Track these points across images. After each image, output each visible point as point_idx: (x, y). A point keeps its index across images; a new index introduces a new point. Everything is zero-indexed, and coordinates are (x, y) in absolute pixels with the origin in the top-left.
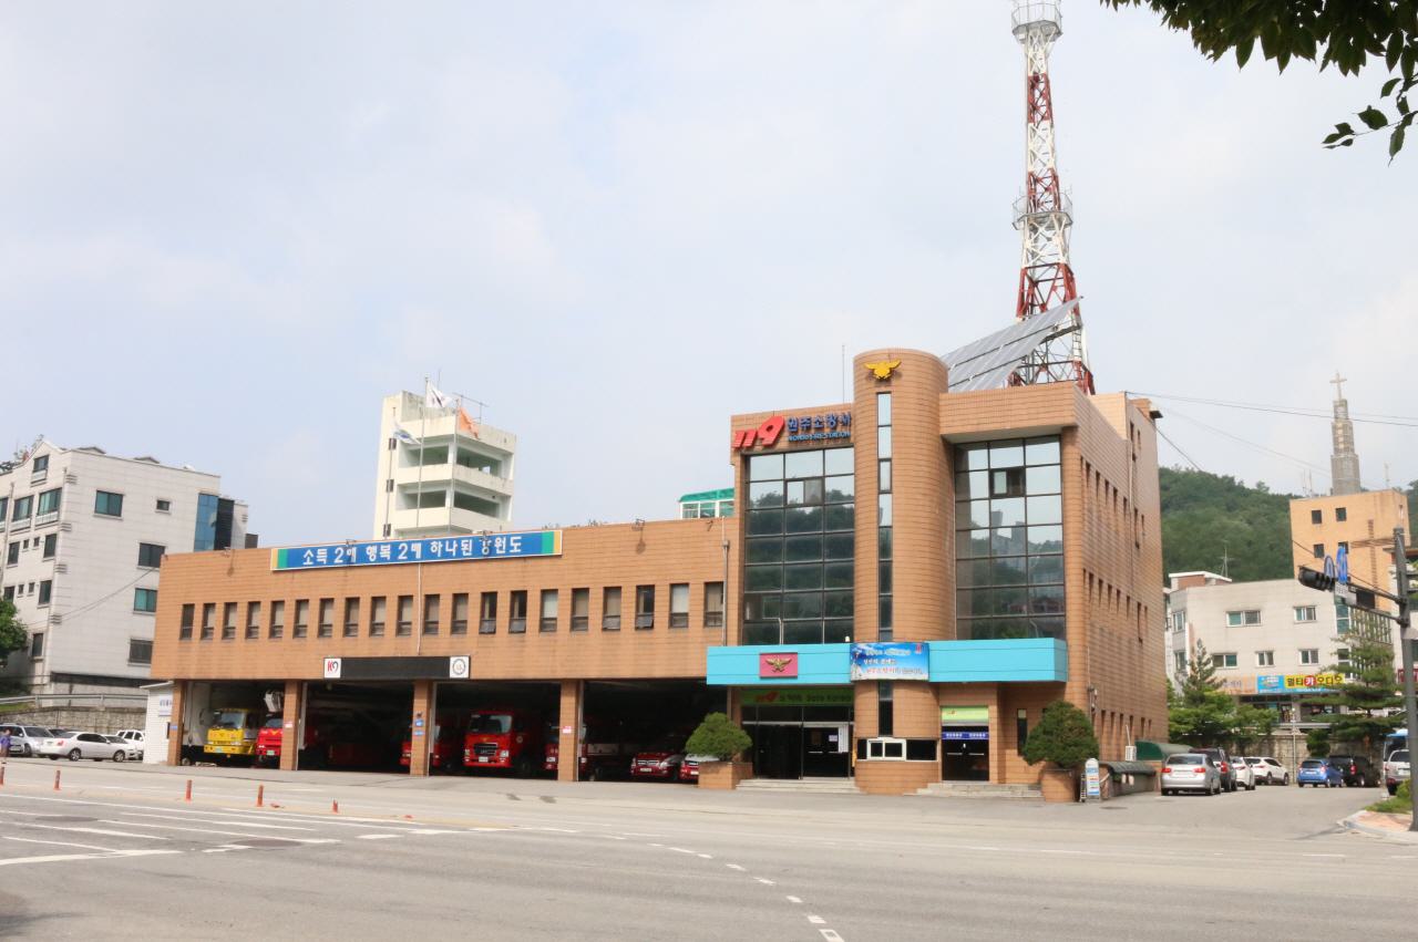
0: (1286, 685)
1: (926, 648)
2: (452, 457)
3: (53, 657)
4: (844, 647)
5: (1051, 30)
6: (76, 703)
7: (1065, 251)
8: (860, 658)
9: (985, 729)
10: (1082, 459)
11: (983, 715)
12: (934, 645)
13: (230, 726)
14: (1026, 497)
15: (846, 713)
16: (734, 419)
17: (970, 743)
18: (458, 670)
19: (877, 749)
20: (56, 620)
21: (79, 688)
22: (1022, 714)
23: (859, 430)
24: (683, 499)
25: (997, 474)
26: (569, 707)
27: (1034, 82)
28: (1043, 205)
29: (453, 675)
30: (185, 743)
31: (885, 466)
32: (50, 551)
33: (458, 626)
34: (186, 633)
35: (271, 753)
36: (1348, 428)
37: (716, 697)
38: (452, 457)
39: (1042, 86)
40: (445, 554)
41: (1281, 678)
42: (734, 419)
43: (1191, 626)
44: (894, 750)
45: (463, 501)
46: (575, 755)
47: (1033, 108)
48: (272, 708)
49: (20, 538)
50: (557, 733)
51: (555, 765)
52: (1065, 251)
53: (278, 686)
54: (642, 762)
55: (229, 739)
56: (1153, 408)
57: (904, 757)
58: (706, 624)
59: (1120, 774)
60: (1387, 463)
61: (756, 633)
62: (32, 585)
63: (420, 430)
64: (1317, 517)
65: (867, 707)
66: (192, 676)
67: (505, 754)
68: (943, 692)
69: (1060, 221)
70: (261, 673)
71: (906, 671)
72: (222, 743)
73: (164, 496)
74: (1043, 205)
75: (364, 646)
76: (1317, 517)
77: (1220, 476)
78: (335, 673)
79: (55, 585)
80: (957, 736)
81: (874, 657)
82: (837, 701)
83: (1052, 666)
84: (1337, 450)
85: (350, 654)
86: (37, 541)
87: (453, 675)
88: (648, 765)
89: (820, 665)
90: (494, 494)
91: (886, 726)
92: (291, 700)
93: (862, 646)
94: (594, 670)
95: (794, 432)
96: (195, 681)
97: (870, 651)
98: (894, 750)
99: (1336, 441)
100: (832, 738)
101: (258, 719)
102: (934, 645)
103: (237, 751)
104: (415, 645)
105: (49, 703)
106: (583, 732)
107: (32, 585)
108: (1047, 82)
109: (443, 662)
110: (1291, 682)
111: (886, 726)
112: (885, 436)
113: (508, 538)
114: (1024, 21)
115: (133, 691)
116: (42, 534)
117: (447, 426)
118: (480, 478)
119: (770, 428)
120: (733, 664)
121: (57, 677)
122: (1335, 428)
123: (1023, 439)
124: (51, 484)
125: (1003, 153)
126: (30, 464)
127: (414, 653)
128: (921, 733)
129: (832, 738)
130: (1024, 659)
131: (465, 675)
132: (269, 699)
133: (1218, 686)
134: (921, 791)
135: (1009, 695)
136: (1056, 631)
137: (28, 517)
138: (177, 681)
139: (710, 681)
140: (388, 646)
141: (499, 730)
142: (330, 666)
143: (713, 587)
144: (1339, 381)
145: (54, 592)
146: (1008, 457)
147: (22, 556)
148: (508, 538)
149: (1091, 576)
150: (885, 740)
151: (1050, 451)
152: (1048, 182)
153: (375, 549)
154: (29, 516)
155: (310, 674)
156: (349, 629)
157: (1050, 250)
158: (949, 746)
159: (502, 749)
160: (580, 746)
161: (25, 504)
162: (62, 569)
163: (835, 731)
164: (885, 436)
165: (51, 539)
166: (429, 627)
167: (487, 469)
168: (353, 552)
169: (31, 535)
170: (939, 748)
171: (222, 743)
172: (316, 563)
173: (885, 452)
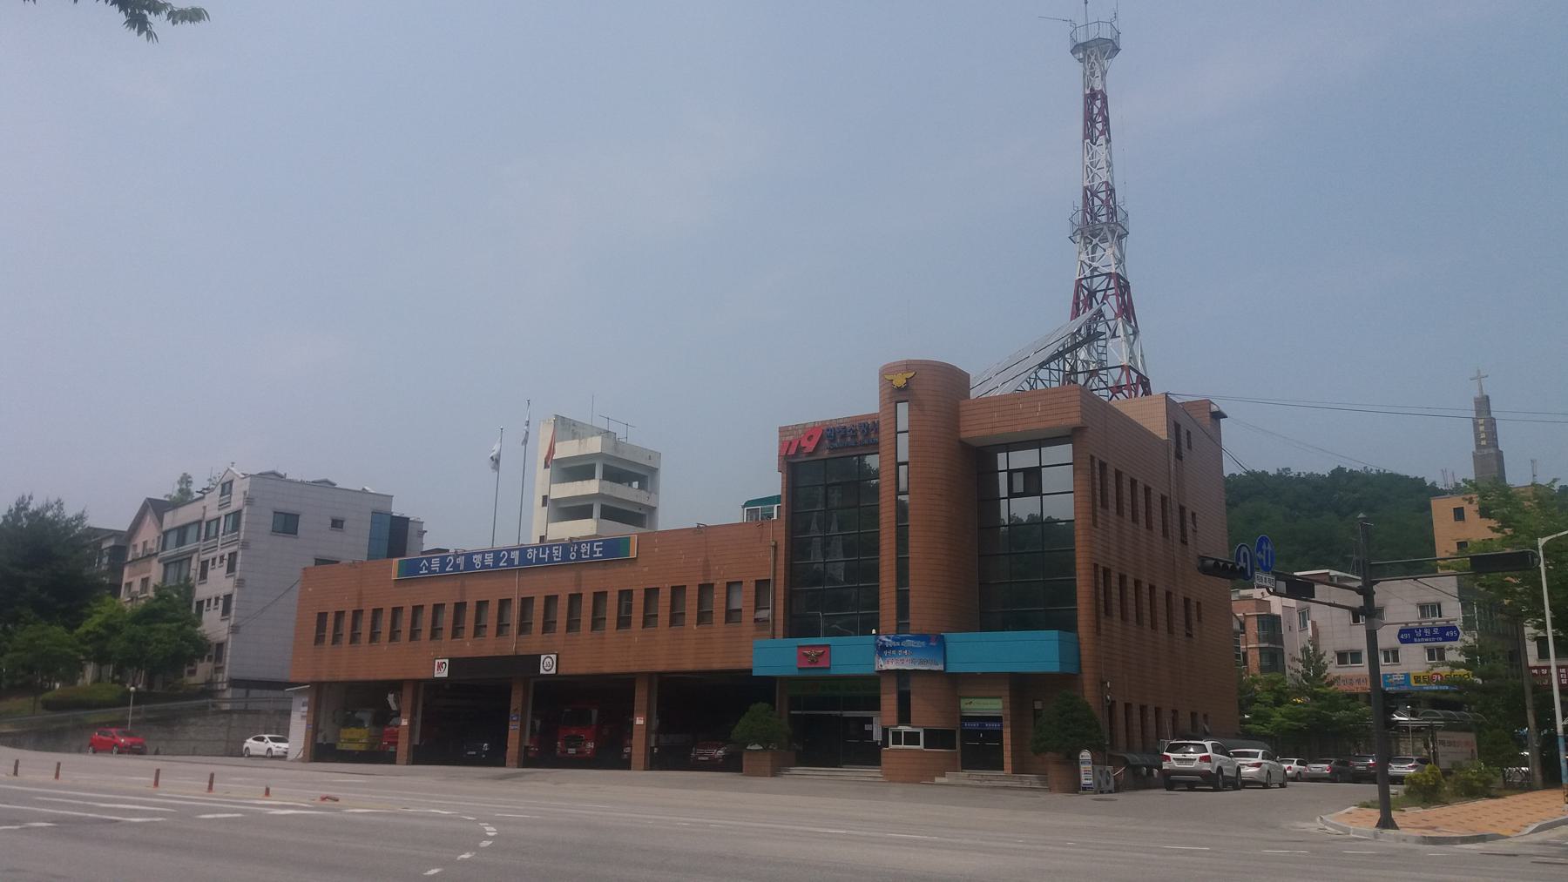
0: (1413, 682)
1: (941, 641)
2: (598, 472)
3: (232, 666)
4: (869, 639)
5: (1110, 48)
6: (252, 706)
7: (1120, 262)
8: (882, 650)
9: (998, 719)
10: (1092, 458)
11: (993, 706)
12: (948, 636)
13: (359, 724)
14: (1042, 495)
15: (875, 704)
16: (782, 430)
17: (986, 732)
18: (548, 665)
19: (897, 736)
20: (235, 629)
21: (254, 693)
22: (1038, 705)
23: (884, 435)
24: (747, 504)
25: (1015, 475)
26: (641, 696)
27: (1092, 97)
28: (1100, 219)
29: (542, 671)
30: (320, 740)
31: (903, 469)
32: (231, 568)
33: (548, 626)
34: (319, 639)
35: (392, 749)
36: (1491, 423)
37: (765, 688)
38: (598, 472)
39: (1098, 103)
40: (539, 560)
41: (1407, 676)
42: (782, 430)
43: (1314, 623)
44: (912, 738)
45: (609, 513)
46: (647, 744)
47: (1089, 119)
48: (394, 707)
49: (209, 556)
50: (632, 723)
51: (630, 755)
52: (1120, 262)
53: (396, 686)
54: (700, 751)
55: (357, 737)
56: (1214, 408)
57: (921, 746)
58: (727, 621)
59: (1140, 767)
60: (1539, 459)
61: (798, 626)
62: (217, 599)
63: (568, 449)
64: (1459, 514)
65: (889, 702)
66: (324, 679)
67: (591, 745)
68: (957, 683)
69: (1113, 232)
70: (382, 674)
71: (921, 662)
72: (350, 741)
73: (338, 515)
74: (1100, 219)
75: (468, 647)
76: (1459, 514)
77: (1272, 472)
78: (443, 673)
79: (234, 598)
80: (975, 725)
81: (893, 648)
82: (865, 692)
83: (1056, 657)
84: (1478, 446)
85: (456, 654)
86: (222, 558)
87: (542, 671)
88: (703, 755)
89: (850, 656)
90: (641, 506)
91: (904, 717)
92: (407, 694)
93: (883, 638)
94: (662, 661)
95: (833, 440)
96: (331, 684)
97: (889, 642)
98: (912, 738)
99: (1478, 439)
100: (867, 727)
101: (384, 717)
102: (948, 636)
103: (363, 748)
104: (511, 645)
105: (227, 707)
106: (655, 723)
107: (217, 599)
108: (1105, 100)
109: (535, 660)
110: (1417, 679)
111: (904, 717)
112: (903, 440)
113: (592, 543)
114: (1081, 39)
115: (279, 694)
116: (226, 552)
117: (594, 445)
118: (629, 493)
119: (810, 438)
120: (774, 656)
121: (234, 683)
122: (1476, 425)
123: (1038, 442)
124: (234, 507)
125: (1062, 172)
126: (218, 490)
127: (470, 654)
128: (938, 723)
129: (867, 727)
130: (1033, 651)
131: (553, 671)
132: (391, 698)
133: (1330, 684)
134: (938, 780)
135: (1021, 686)
136: (1066, 624)
137: (166, 533)
138: (312, 683)
139: (755, 673)
140: (490, 646)
141: (579, 723)
142: (440, 666)
143: (762, 585)
144: (1479, 377)
145: (234, 605)
146: (1024, 459)
147: (210, 573)
148: (592, 543)
149: (1106, 572)
150: (904, 729)
151: (1064, 452)
152: (1103, 196)
153: (479, 557)
154: (216, 536)
155: (422, 674)
156: (457, 631)
157: (1106, 259)
158: (967, 735)
159: (587, 740)
160: (653, 737)
161: (213, 525)
162: (240, 583)
163: (870, 721)
164: (903, 440)
165: (233, 555)
166: (524, 628)
167: (635, 484)
168: (461, 560)
169: (219, 552)
170: (958, 737)
171: (350, 741)
172: (430, 571)
173: (903, 456)
